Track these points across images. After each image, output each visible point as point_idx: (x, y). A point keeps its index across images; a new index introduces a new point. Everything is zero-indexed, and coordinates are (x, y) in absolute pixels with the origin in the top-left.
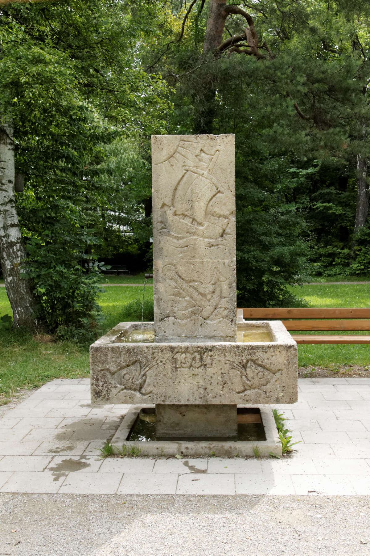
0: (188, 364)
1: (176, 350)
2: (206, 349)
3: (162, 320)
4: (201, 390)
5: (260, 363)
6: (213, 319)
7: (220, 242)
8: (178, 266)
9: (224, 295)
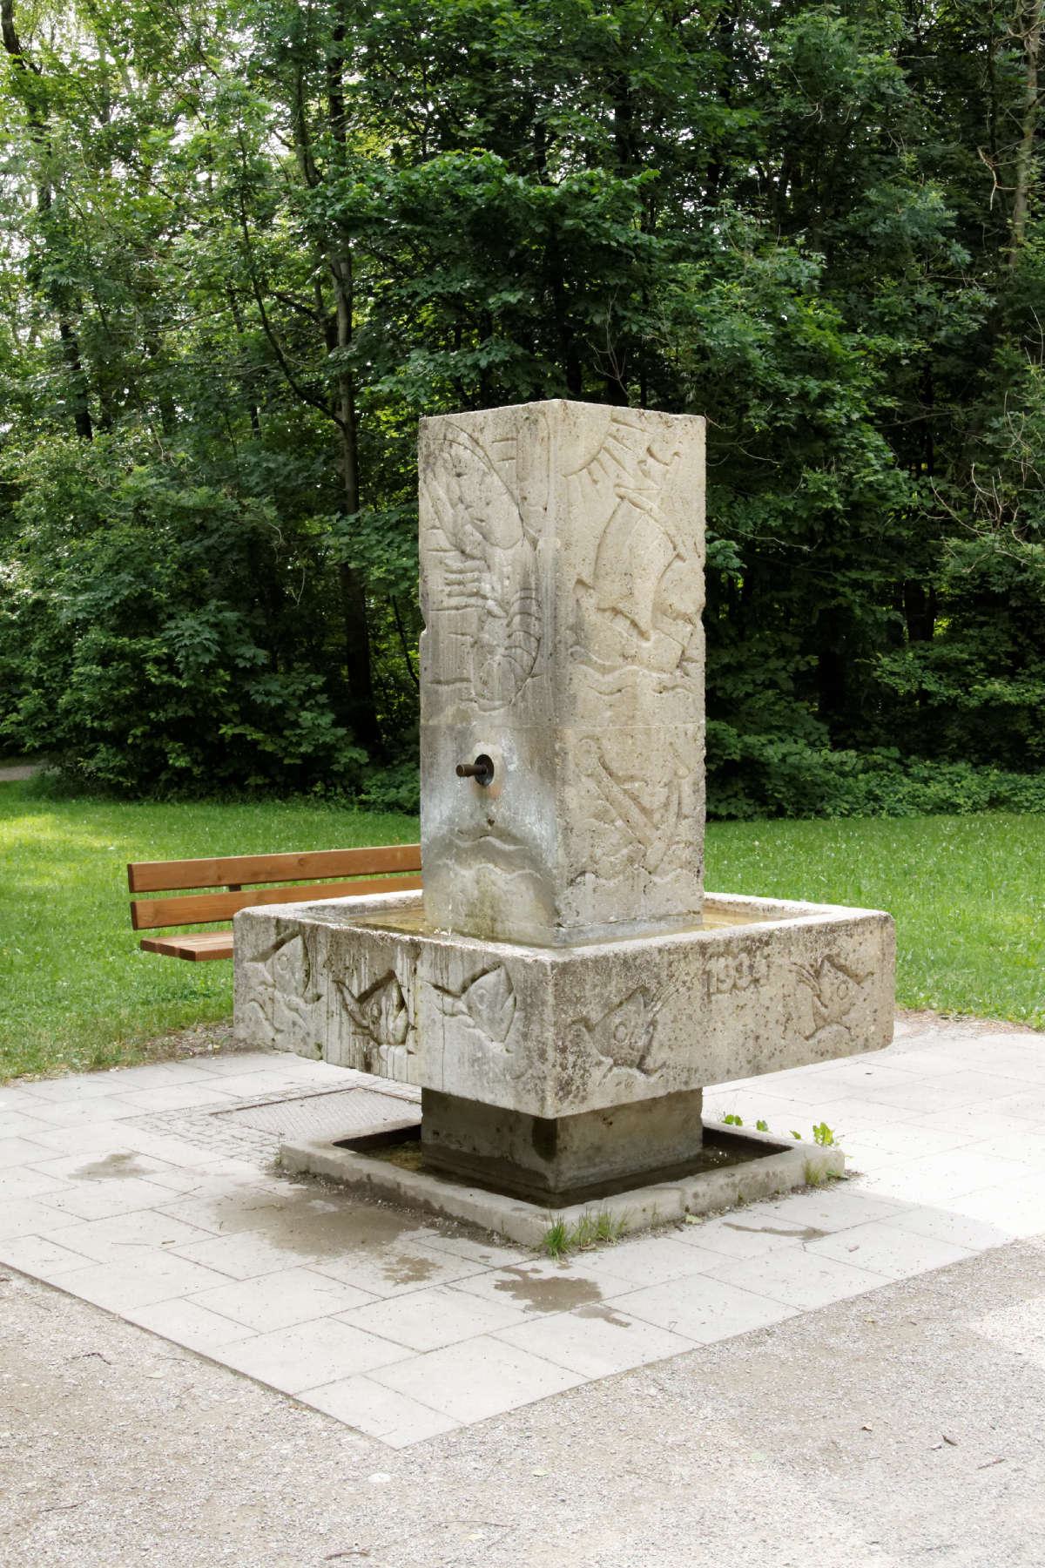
0: (729, 983)
1: (710, 951)
2: (760, 940)
3: (572, 882)
4: (751, 1042)
5: (842, 961)
6: (666, 873)
7: (679, 681)
8: (604, 741)
9: (686, 810)
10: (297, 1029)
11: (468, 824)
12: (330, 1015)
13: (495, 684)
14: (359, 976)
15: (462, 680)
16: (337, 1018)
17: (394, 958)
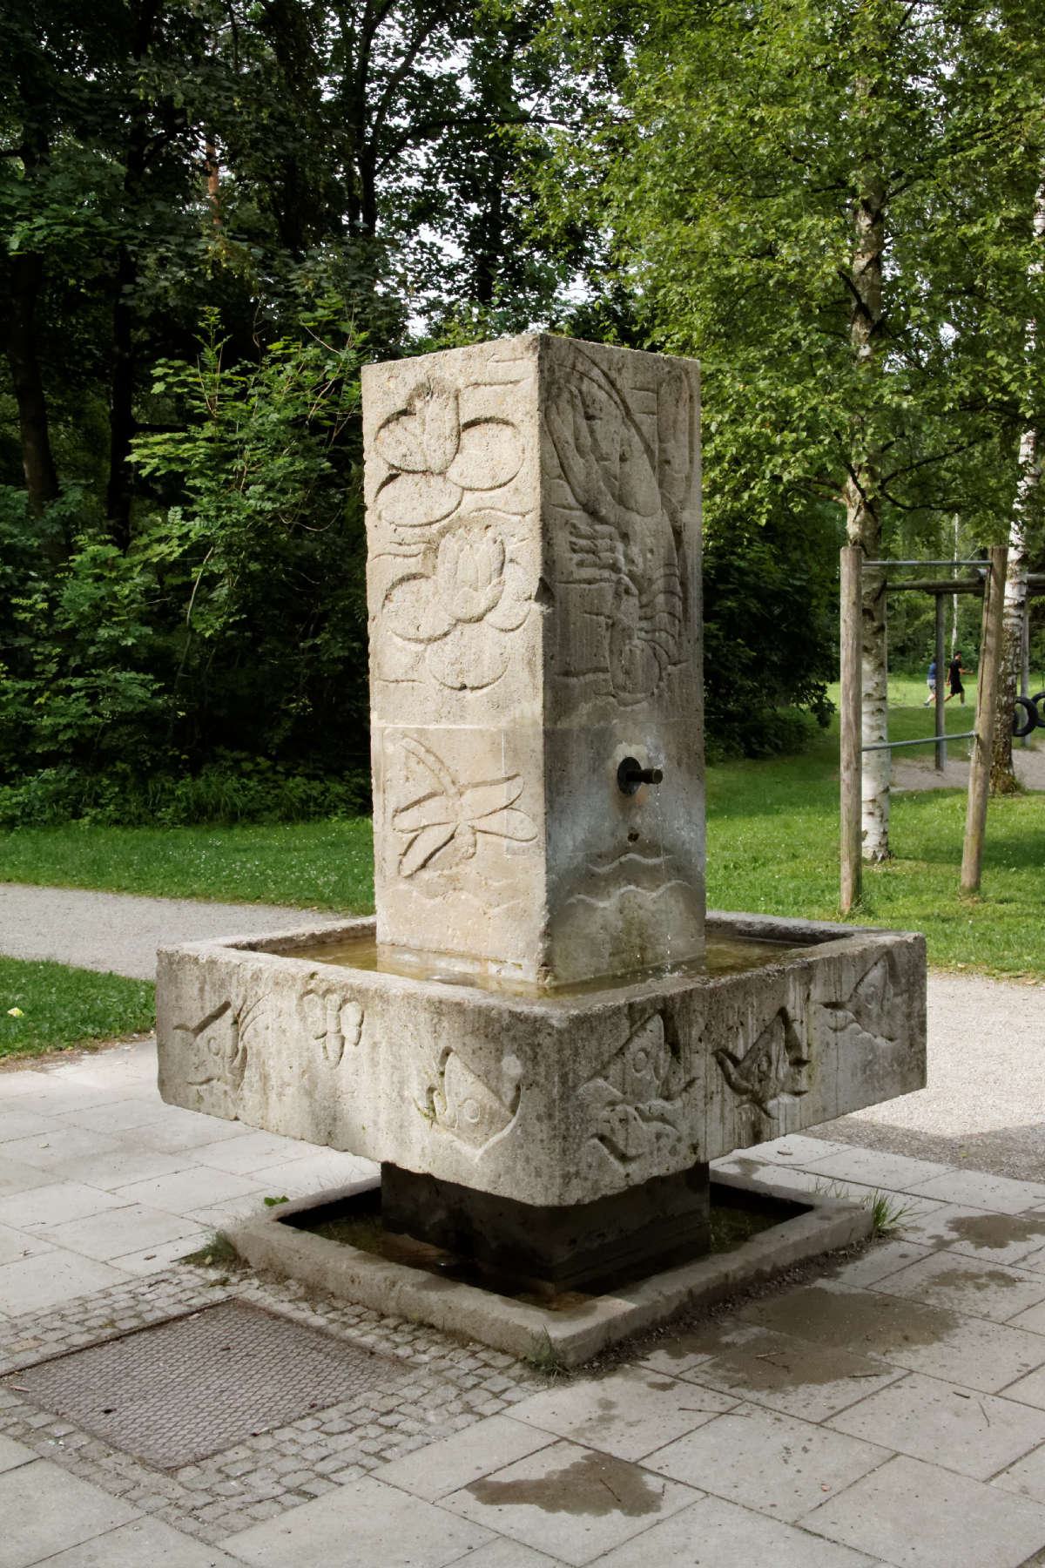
10: (663, 1141)
11: (607, 844)
12: (709, 1098)
13: (640, 675)
14: (746, 1032)
15: (597, 670)
16: (717, 1098)
17: (785, 993)
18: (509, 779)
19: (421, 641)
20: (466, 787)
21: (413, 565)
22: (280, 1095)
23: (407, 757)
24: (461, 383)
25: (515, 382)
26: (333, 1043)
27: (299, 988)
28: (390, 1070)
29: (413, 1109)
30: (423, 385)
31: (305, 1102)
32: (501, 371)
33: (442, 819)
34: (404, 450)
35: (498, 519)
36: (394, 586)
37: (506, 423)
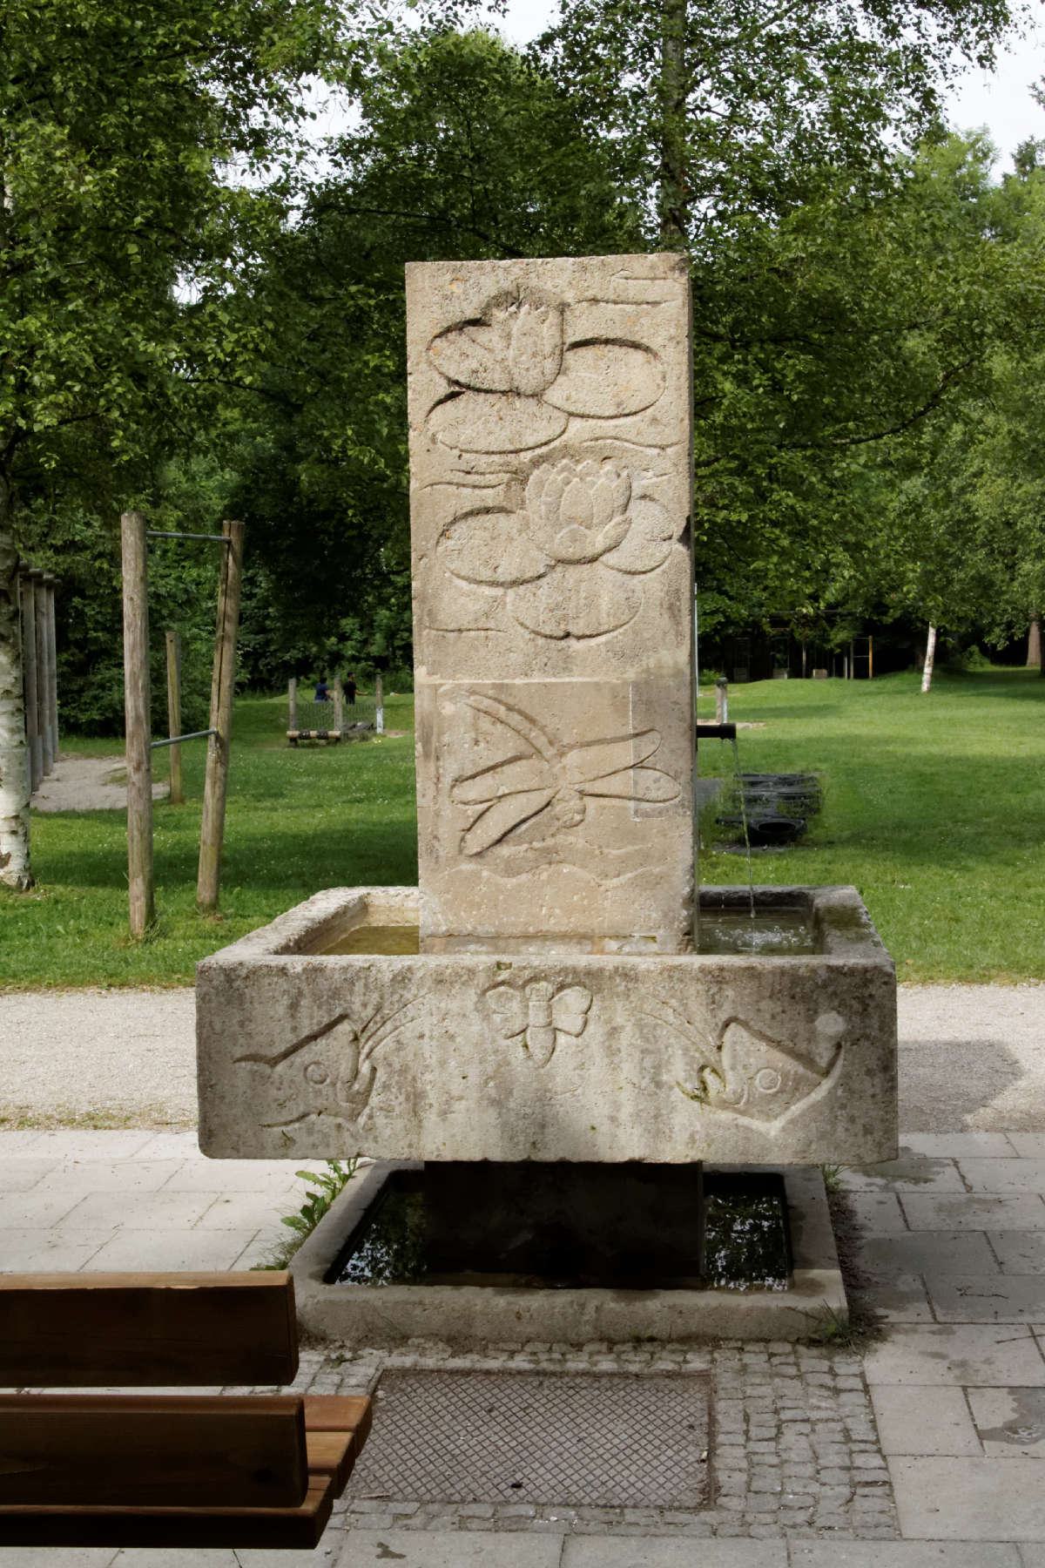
18: (637, 735)
19: (502, 584)
20: (571, 747)
21: (490, 497)
22: (444, 1114)
23: (476, 718)
24: (569, 297)
25: (655, 303)
26: (538, 1040)
27: (482, 980)
28: (637, 1055)
29: (677, 1094)
30: (508, 293)
31: (491, 1115)
32: (654, 291)
33: (534, 784)
34: (475, 365)
35: (626, 450)
36: (455, 520)
37: (647, 349)
